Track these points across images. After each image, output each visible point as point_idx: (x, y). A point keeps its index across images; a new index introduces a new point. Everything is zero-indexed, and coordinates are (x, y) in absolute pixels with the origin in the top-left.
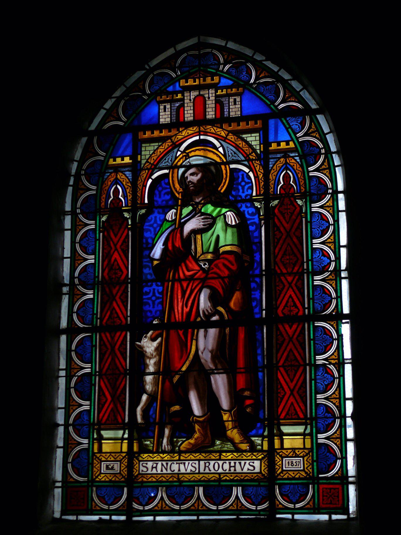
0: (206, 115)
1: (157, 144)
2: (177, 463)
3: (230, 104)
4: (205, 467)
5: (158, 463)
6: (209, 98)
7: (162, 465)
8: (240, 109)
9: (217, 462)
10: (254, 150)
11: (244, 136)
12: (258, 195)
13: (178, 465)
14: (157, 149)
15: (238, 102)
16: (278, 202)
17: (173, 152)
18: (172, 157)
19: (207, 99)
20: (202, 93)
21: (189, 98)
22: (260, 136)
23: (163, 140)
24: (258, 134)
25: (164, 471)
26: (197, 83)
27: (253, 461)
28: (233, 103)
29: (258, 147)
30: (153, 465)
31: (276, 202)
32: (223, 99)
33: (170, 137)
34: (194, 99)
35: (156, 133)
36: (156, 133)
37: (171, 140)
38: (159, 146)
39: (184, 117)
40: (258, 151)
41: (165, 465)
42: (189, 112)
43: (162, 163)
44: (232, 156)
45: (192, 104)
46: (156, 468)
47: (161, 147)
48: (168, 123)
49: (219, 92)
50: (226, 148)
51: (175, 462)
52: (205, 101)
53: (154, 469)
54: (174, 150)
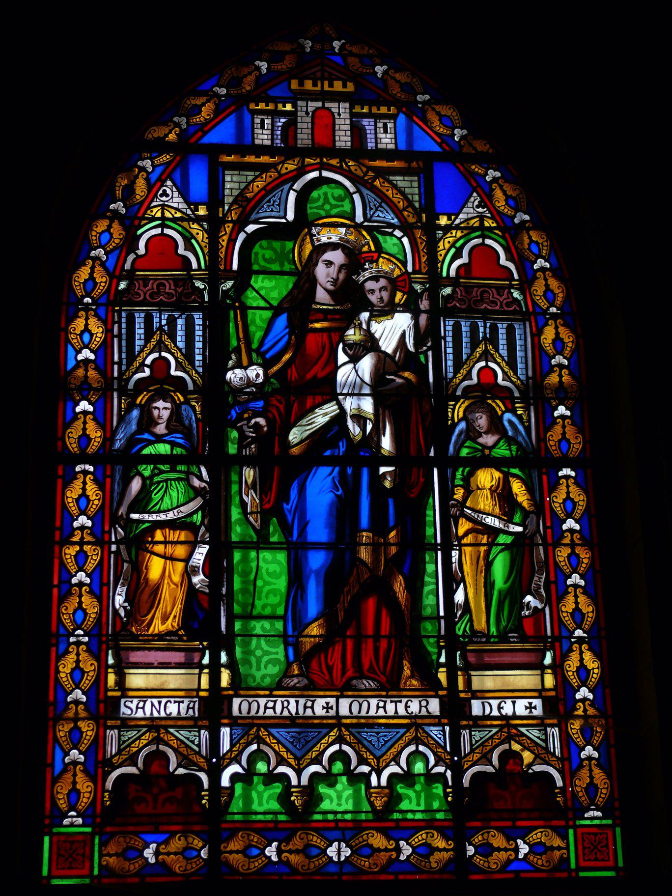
0: (334, 141)
1: (253, 173)
2: (175, 702)
3: (378, 131)
4: (283, 708)
5: (277, 700)
6: (339, 114)
7: (153, 705)
8: (310, 135)
9: (366, 701)
10: (410, 203)
11: (391, 178)
12: (416, 271)
13: (394, 703)
14: (253, 181)
15: (268, 124)
16: (233, 286)
17: (282, 191)
18: (280, 199)
19: (336, 116)
20: (327, 105)
21: (304, 109)
22: (419, 181)
23: (263, 168)
24: (416, 178)
25: (156, 714)
26: (319, 88)
27: (131, 700)
28: (259, 126)
29: (417, 198)
30: (378, 703)
31: (230, 284)
32: (365, 122)
33: (274, 166)
34: (313, 112)
35: (252, 159)
36: (252, 159)
37: (276, 169)
38: (257, 177)
39: (296, 139)
40: (417, 205)
41: (157, 705)
42: (343, 133)
43: (263, 207)
44: (273, 205)
45: (309, 119)
46: (143, 708)
47: (259, 179)
48: (308, 147)
49: (357, 109)
50: (365, 195)
51: (172, 700)
52: (334, 119)
53: (140, 711)
54: (285, 187)
